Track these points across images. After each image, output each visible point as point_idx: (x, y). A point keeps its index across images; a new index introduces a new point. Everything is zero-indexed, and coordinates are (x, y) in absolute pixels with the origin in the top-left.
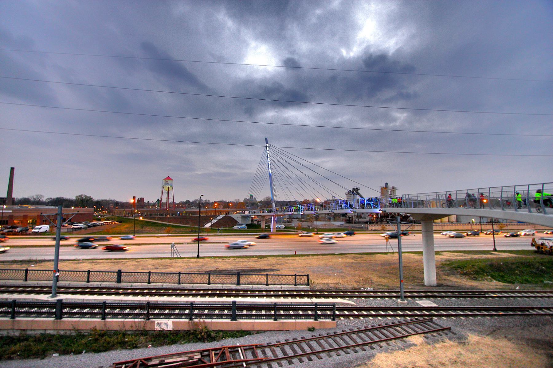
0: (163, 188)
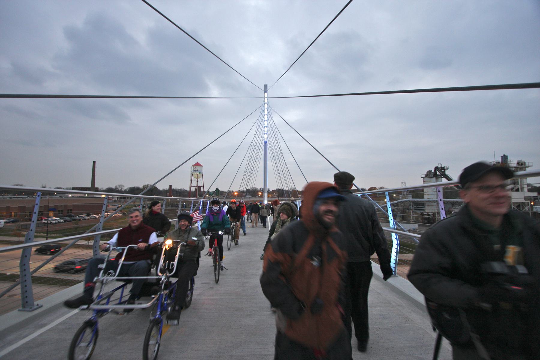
0: (192, 175)
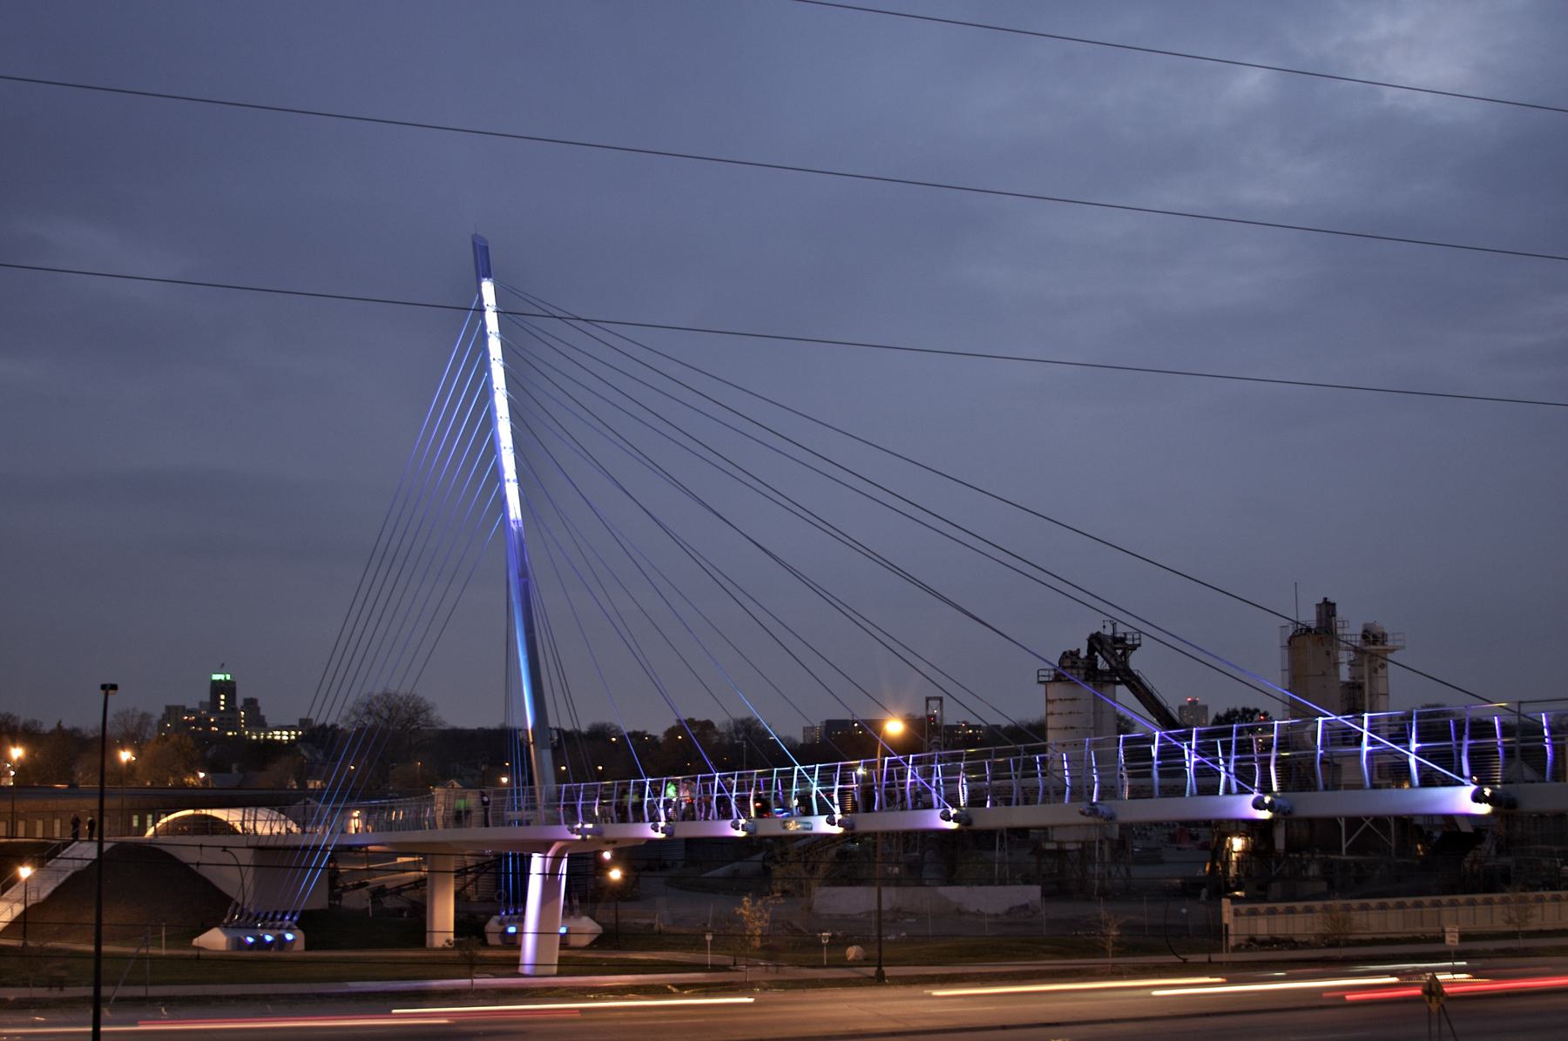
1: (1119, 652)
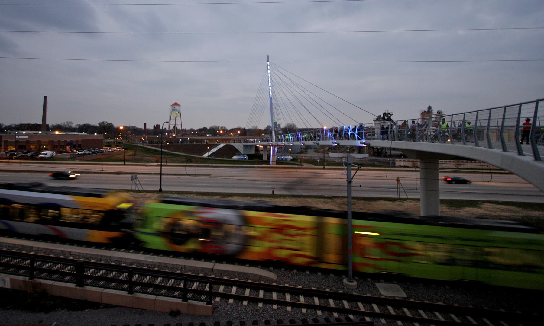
0: (171, 114)
1: (389, 116)
